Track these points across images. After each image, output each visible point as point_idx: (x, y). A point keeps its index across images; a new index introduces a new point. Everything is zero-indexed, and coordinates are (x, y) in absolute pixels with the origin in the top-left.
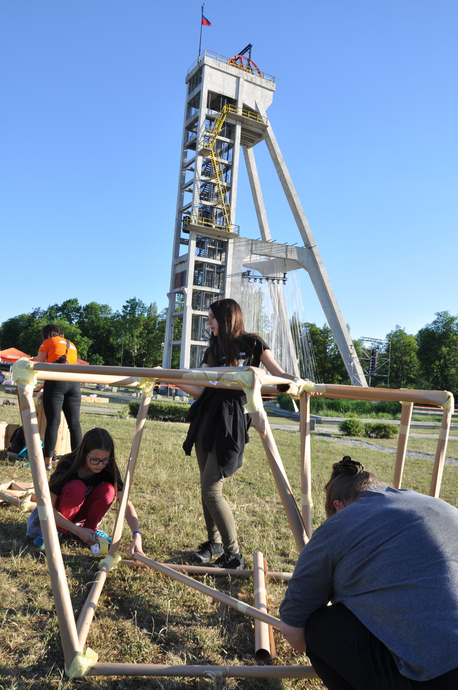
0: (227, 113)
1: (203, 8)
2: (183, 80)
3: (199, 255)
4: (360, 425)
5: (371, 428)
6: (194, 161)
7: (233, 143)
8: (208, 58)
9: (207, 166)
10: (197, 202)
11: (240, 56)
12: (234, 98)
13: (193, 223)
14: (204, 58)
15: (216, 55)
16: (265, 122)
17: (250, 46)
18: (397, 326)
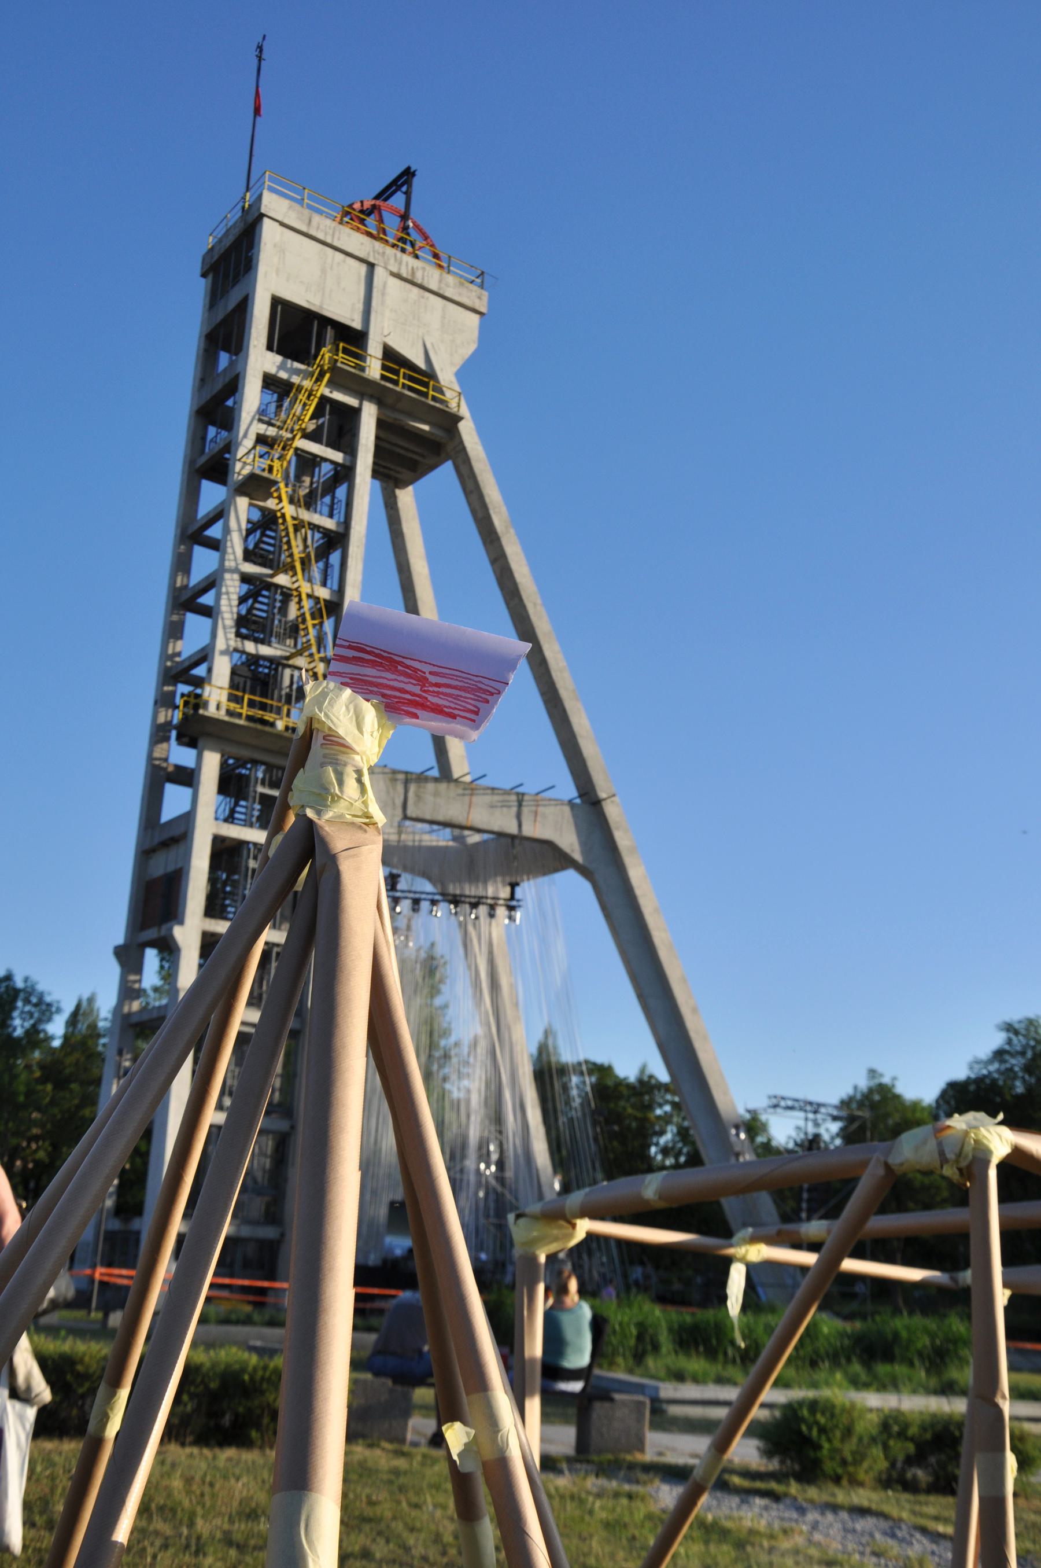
0: (334, 369)
1: (260, 48)
2: (197, 268)
3: (230, 819)
4: (860, 1427)
5: (912, 1439)
6: (220, 514)
7: (348, 463)
8: (274, 196)
9: (263, 535)
10: (225, 638)
11: (378, 202)
12: (357, 324)
13: (211, 711)
14: (260, 198)
15: (297, 189)
16: (453, 404)
17: (408, 175)
18: (872, 1073)
